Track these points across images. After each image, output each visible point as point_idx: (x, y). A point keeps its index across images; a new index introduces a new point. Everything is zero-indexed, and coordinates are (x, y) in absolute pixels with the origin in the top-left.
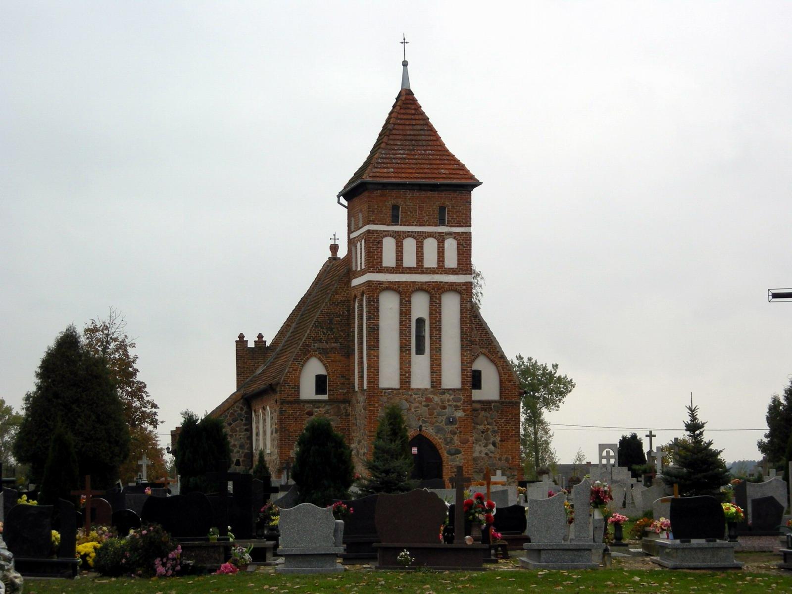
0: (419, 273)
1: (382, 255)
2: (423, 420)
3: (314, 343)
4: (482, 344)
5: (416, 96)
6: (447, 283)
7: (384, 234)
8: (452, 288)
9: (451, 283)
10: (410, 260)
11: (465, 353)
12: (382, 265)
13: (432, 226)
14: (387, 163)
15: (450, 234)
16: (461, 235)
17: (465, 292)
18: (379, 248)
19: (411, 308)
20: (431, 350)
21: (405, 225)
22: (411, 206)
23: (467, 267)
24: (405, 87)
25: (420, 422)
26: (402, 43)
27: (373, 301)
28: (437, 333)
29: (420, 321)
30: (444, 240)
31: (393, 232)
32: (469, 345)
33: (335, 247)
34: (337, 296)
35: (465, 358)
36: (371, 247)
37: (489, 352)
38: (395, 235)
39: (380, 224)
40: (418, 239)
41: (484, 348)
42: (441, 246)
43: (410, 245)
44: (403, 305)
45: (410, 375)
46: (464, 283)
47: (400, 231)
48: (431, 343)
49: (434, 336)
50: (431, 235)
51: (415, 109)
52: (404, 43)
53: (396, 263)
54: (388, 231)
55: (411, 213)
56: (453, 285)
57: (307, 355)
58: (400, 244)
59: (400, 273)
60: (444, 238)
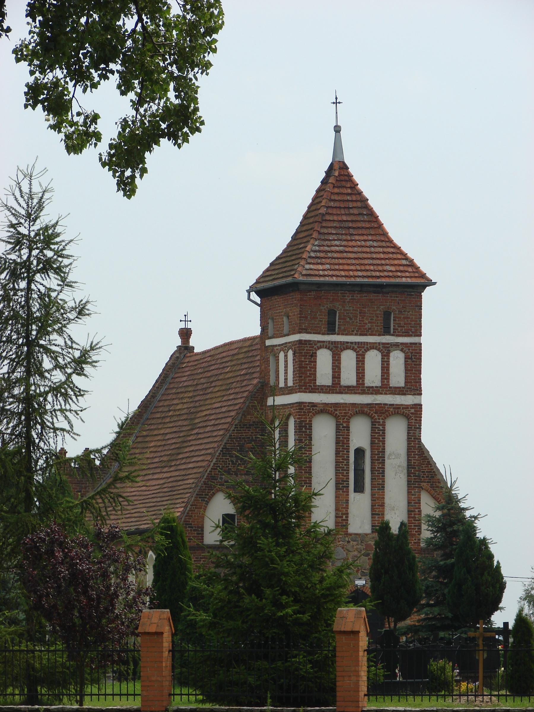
0: (359, 393)
1: (315, 371)
2: (363, 572)
3: (221, 475)
4: (423, 477)
5: (351, 170)
6: (393, 405)
7: (319, 345)
8: (398, 411)
9: (397, 405)
10: (348, 377)
11: (413, 491)
12: (316, 383)
13: (375, 335)
14: (322, 258)
15: (396, 346)
16: (408, 347)
17: (413, 416)
18: (312, 362)
19: (349, 435)
20: (372, 487)
21: (343, 334)
22: (350, 310)
23: (416, 386)
24: (337, 159)
25: (359, 574)
26: (334, 103)
27: (305, 427)
28: (380, 466)
29: (359, 452)
30: (389, 353)
31: (329, 343)
32: (416, 482)
33: (187, 332)
34: (249, 417)
35: (413, 497)
36: (303, 361)
37: (431, 487)
38: (331, 346)
39: (314, 333)
40: (358, 352)
41: (425, 482)
42: (386, 360)
43: (348, 359)
44: (340, 432)
45: (347, 517)
46: (412, 405)
47: (338, 342)
48: (372, 479)
49: (377, 471)
50: (373, 347)
51: (351, 188)
52: (336, 103)
53: (333, 381)
54: (324, 342)
55: (351, 319)
56: (400, 408)
57: (212, 490)
58: (337, 358)
59: (337, 393)
60: (389, 350)
